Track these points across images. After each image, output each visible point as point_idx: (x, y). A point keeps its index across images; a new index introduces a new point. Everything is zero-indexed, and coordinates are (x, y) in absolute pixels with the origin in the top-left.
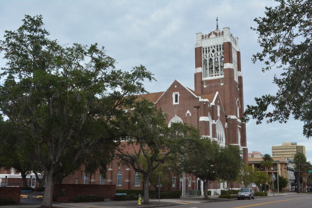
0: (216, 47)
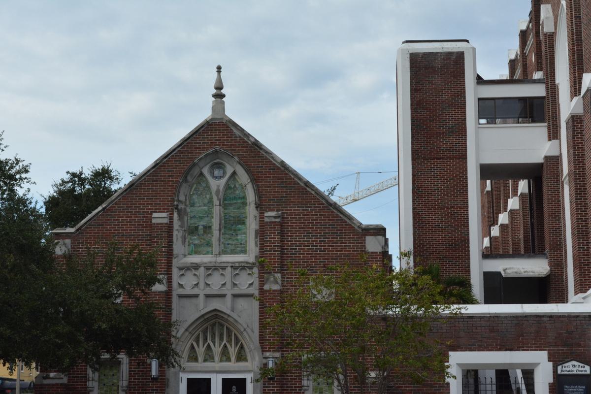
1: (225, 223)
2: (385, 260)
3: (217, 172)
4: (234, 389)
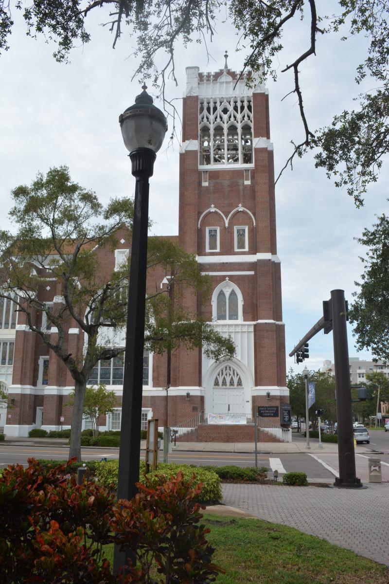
0: (232, 103)
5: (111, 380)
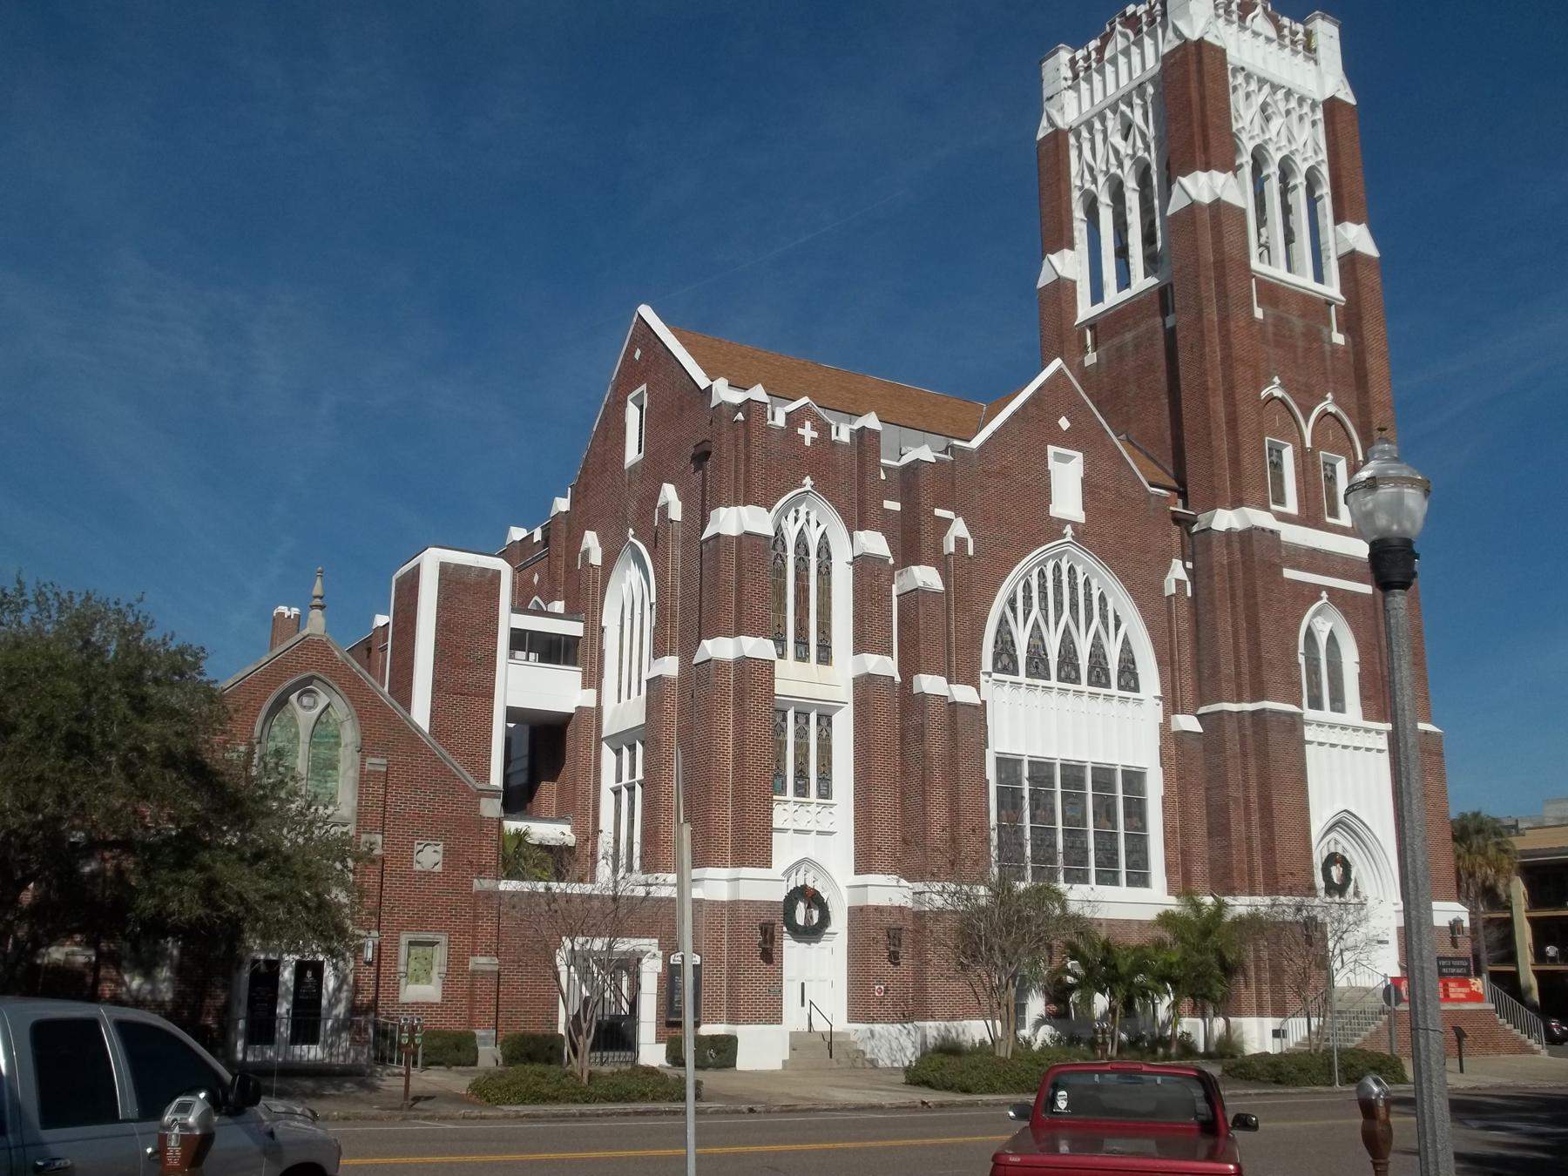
1: (313, 765)
2: (272, 765)
3: (306, 700)
4: (309, 974)
5: (1092, 867)
